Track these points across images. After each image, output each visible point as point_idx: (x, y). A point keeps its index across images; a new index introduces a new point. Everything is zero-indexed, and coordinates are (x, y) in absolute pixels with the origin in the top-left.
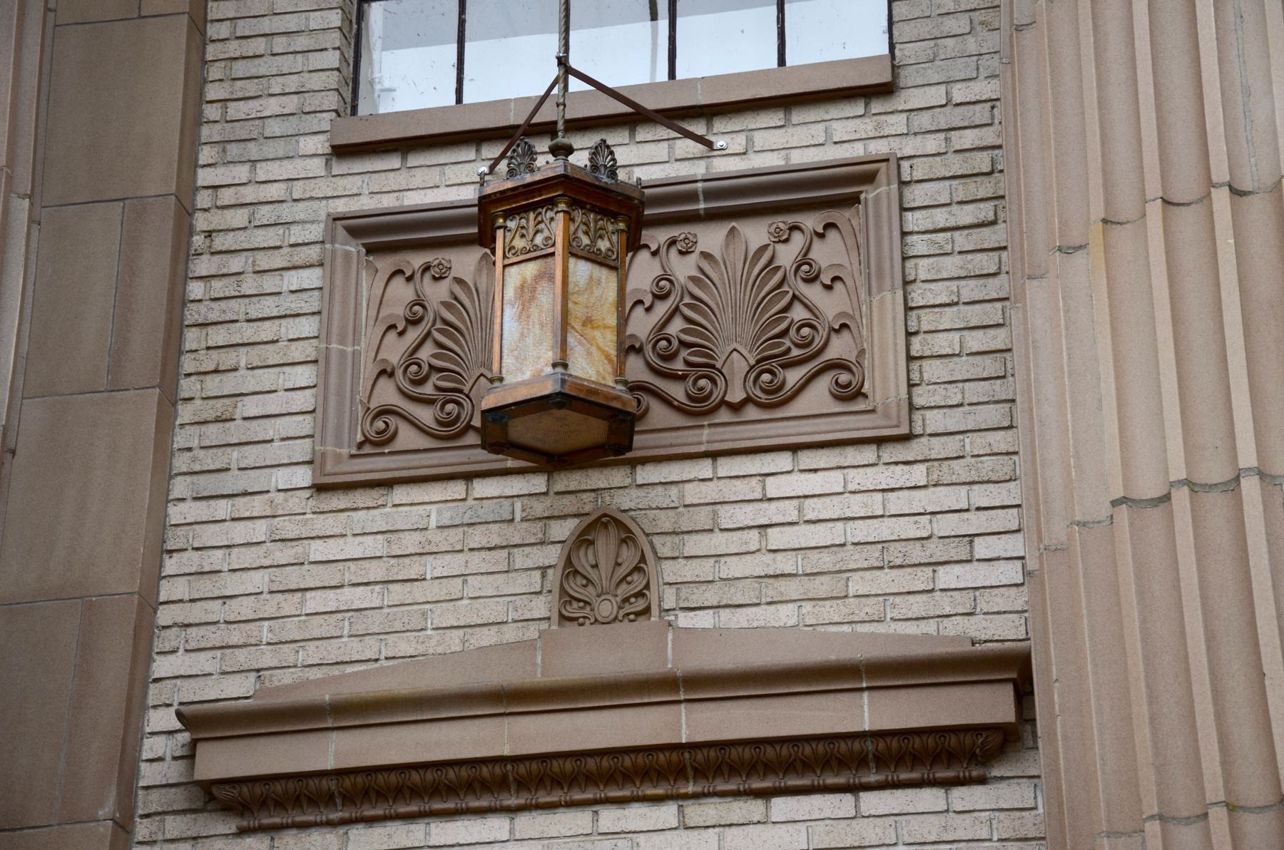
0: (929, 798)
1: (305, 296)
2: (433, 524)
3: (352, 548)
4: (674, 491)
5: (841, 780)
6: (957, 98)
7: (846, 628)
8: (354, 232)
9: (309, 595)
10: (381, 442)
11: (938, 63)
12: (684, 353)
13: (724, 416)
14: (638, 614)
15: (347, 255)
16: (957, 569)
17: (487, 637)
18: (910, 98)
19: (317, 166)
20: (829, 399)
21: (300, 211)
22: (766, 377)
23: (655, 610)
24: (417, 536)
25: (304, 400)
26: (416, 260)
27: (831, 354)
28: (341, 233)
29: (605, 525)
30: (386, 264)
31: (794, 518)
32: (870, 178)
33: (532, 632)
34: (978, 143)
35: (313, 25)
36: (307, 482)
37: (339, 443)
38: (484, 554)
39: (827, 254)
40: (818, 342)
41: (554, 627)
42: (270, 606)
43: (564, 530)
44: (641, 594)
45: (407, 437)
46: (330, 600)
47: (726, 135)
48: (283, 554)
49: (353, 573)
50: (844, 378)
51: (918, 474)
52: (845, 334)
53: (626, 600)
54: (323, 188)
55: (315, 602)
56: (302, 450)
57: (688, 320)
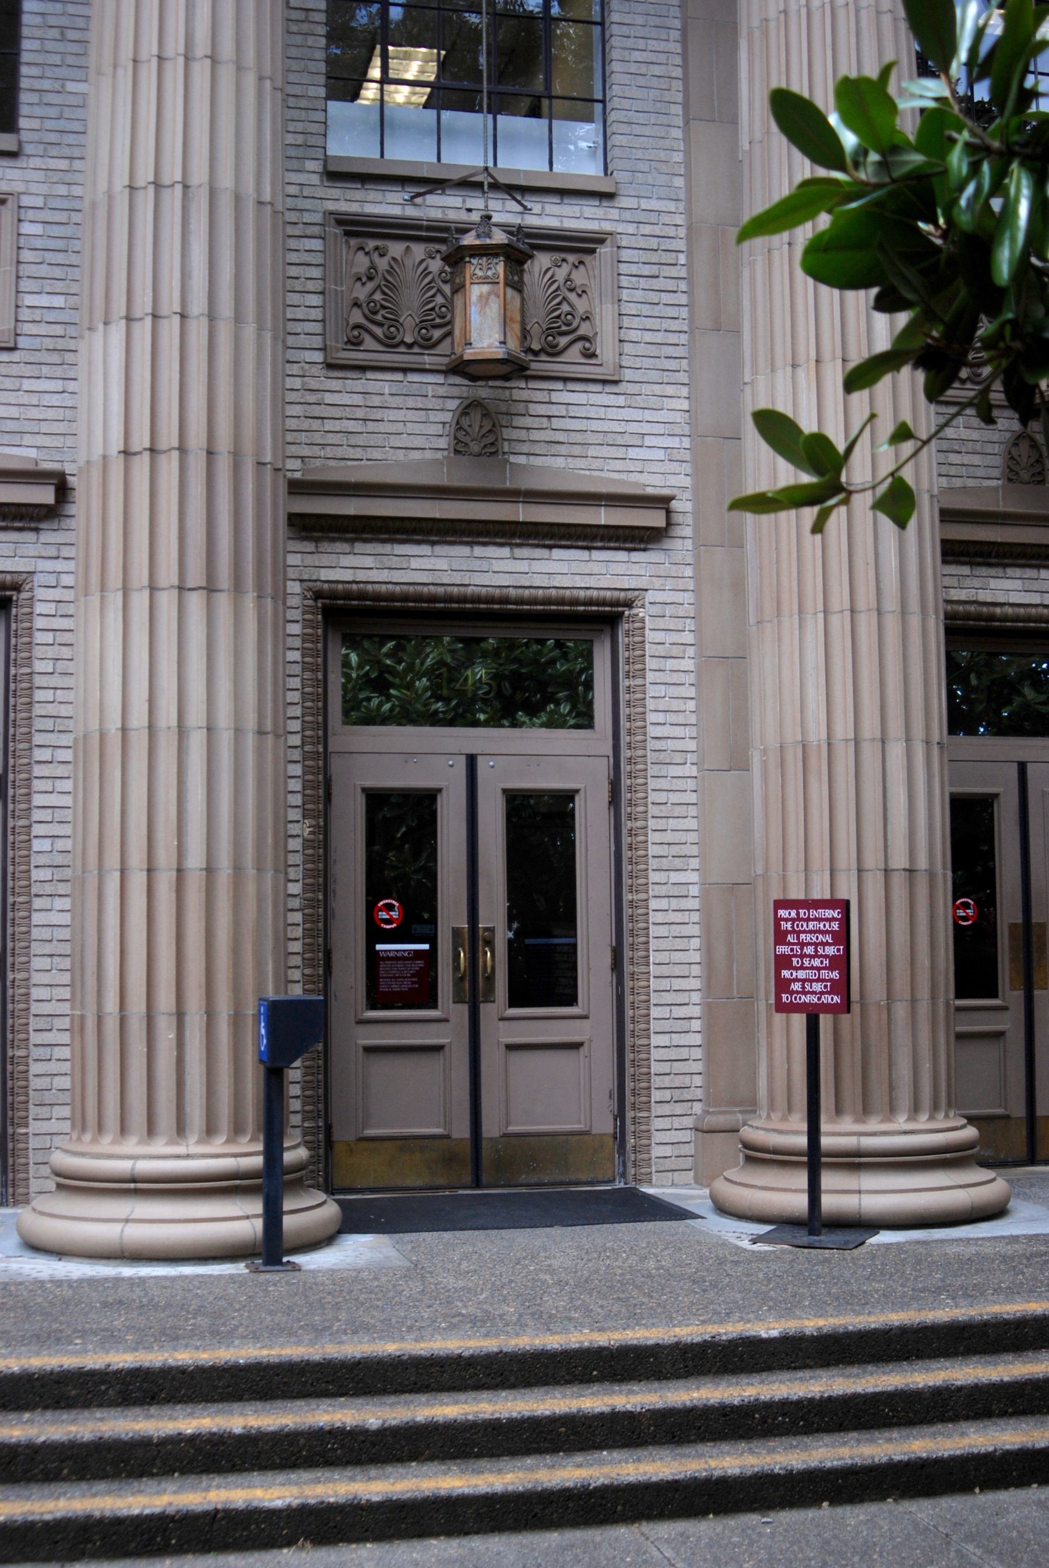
0: (622, 555)
1: (313, 254)
2: (387, 391)
3: (346, 399)
4: (507, 392)
5: (584, 544)
6: (643, 207)
7: (587, 473)
8: (340, 222)
9: (326, 421)
10: (355, 343)
11: (634, 185)
12: (383, 312)
13: (402, 349)
14: (492, 454)
15: (336, 234)
16: (637, 449)
17: (416, 455)
18: (623, 202)
19: (315, 179)
20: (579, 354)
21: (307, 204)
22: (424, 331)
23: (500, 452)
24: (379, 398)
25: (317, 314)
26: (371, 244)
27: (581, 332)
28: (333, 222)
29: (476, 406)
30: (354, 242)
31: (564, 414)
32: (602, 241)
33: (439, 455)
34: (652, 233)
35: (310, 94)
36: (321, 360)
37: (337, 342)
38: (414, 412)
39: (579, 277)
40: (575, 325)
41: (452, 455)
42: (306, 424)
43: (453, 404)
44: (492, 444)
45: (369, 343)
46: (337, 425)
47: (534, 204)
48: (311, 398)
49: (347, 412)
50: (587, 345)
51: (621, 400)
52: (587, 322)
53: (485, 446)
54: (320, 192)
55: (329, 425)
56: (317, 341)
57: (384, 293)
